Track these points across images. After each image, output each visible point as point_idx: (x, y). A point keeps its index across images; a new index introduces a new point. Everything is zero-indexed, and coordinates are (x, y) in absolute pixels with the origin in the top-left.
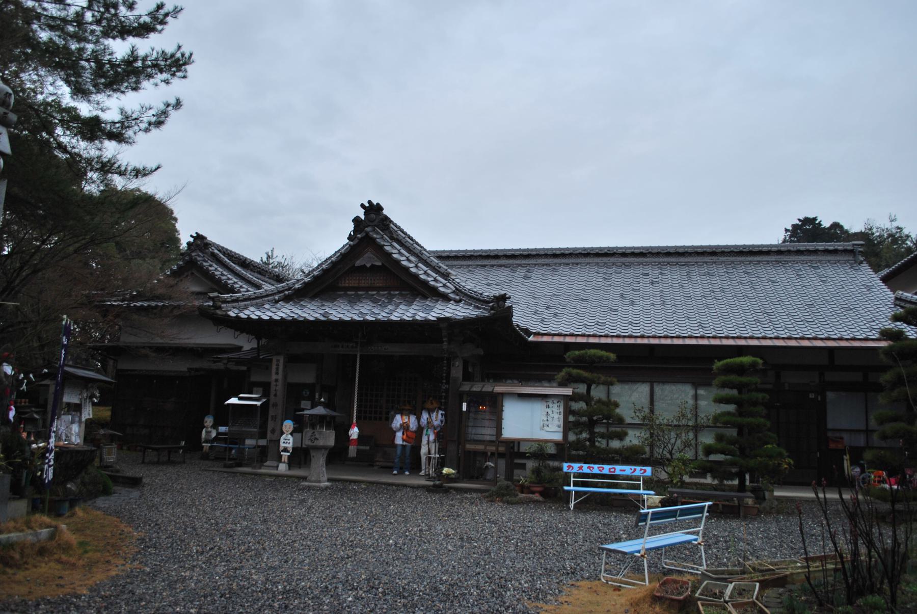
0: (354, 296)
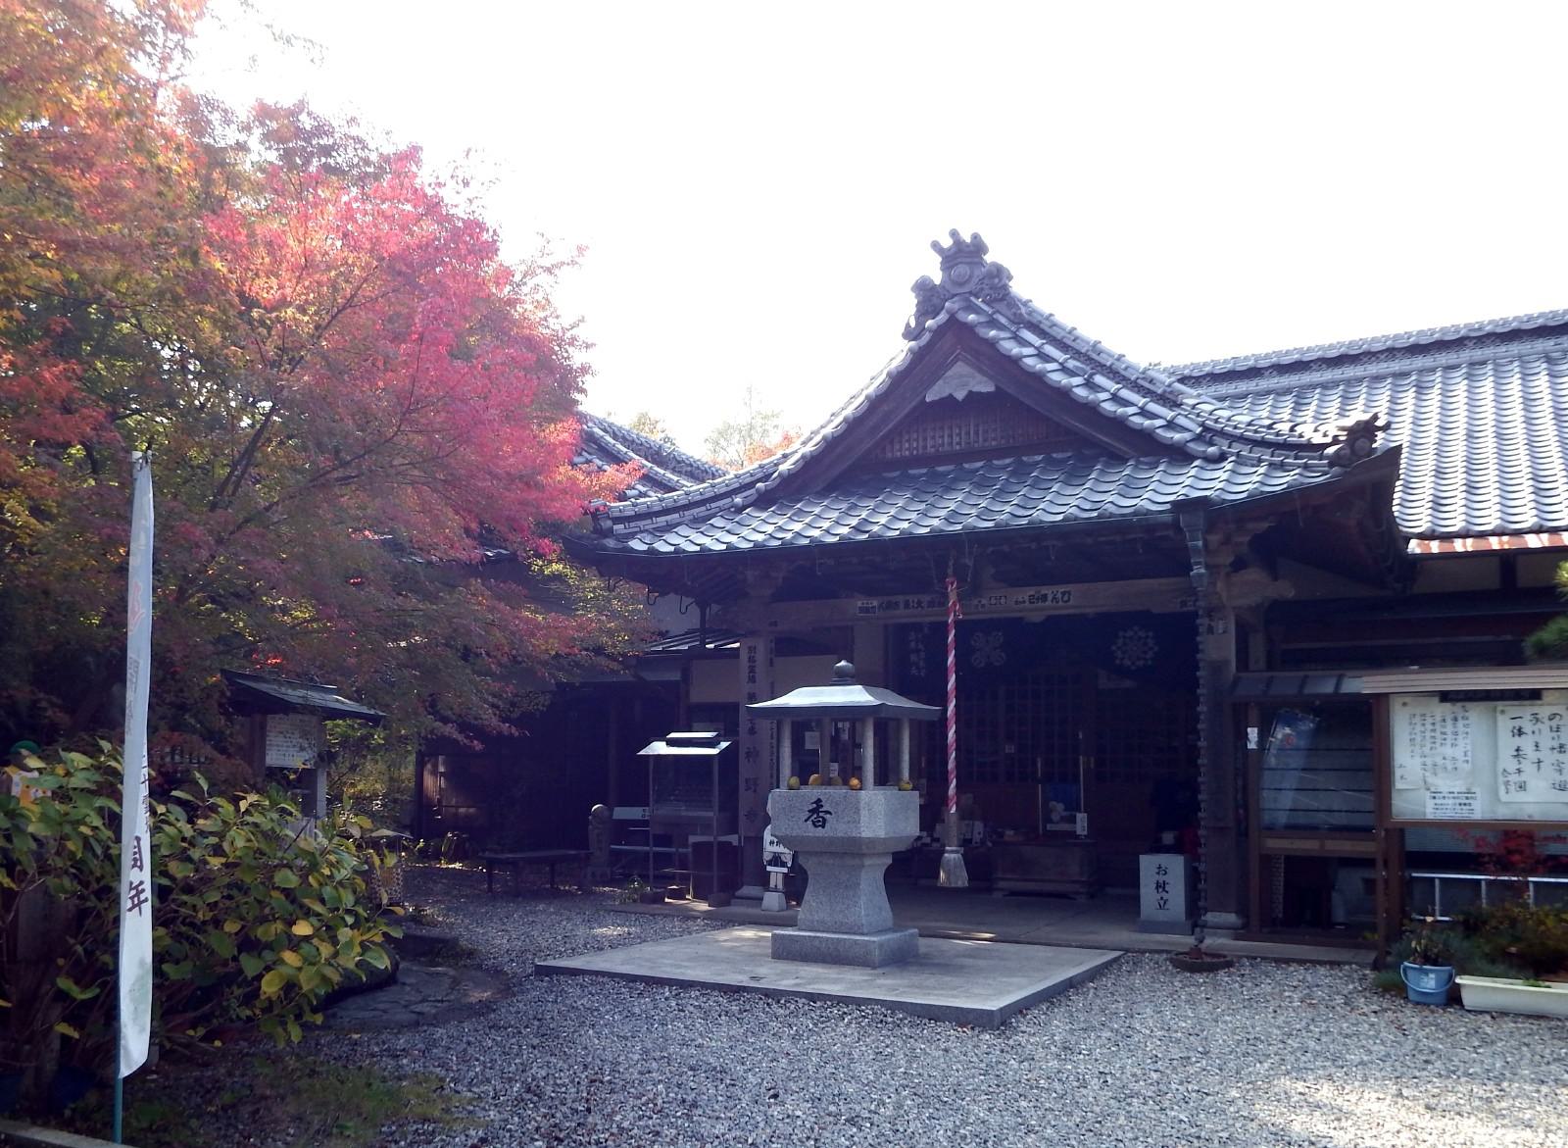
0: (926, 475)
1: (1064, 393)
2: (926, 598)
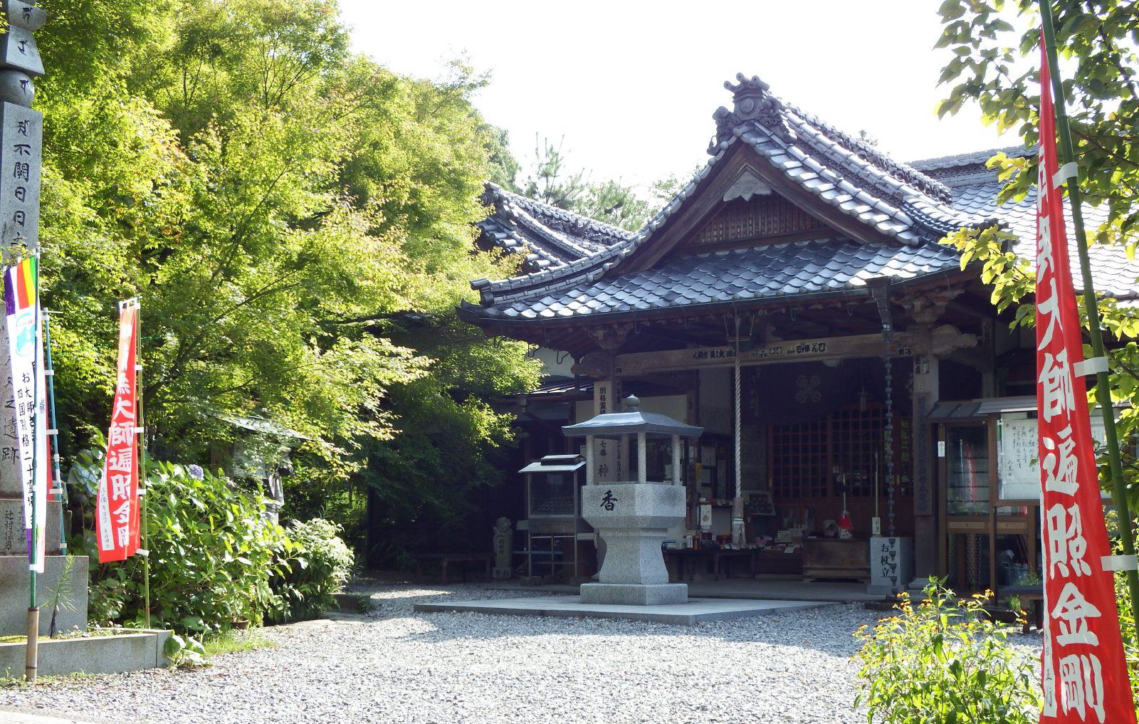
0: (722, 257)
1: (814, 196)
2: (726, 349)
